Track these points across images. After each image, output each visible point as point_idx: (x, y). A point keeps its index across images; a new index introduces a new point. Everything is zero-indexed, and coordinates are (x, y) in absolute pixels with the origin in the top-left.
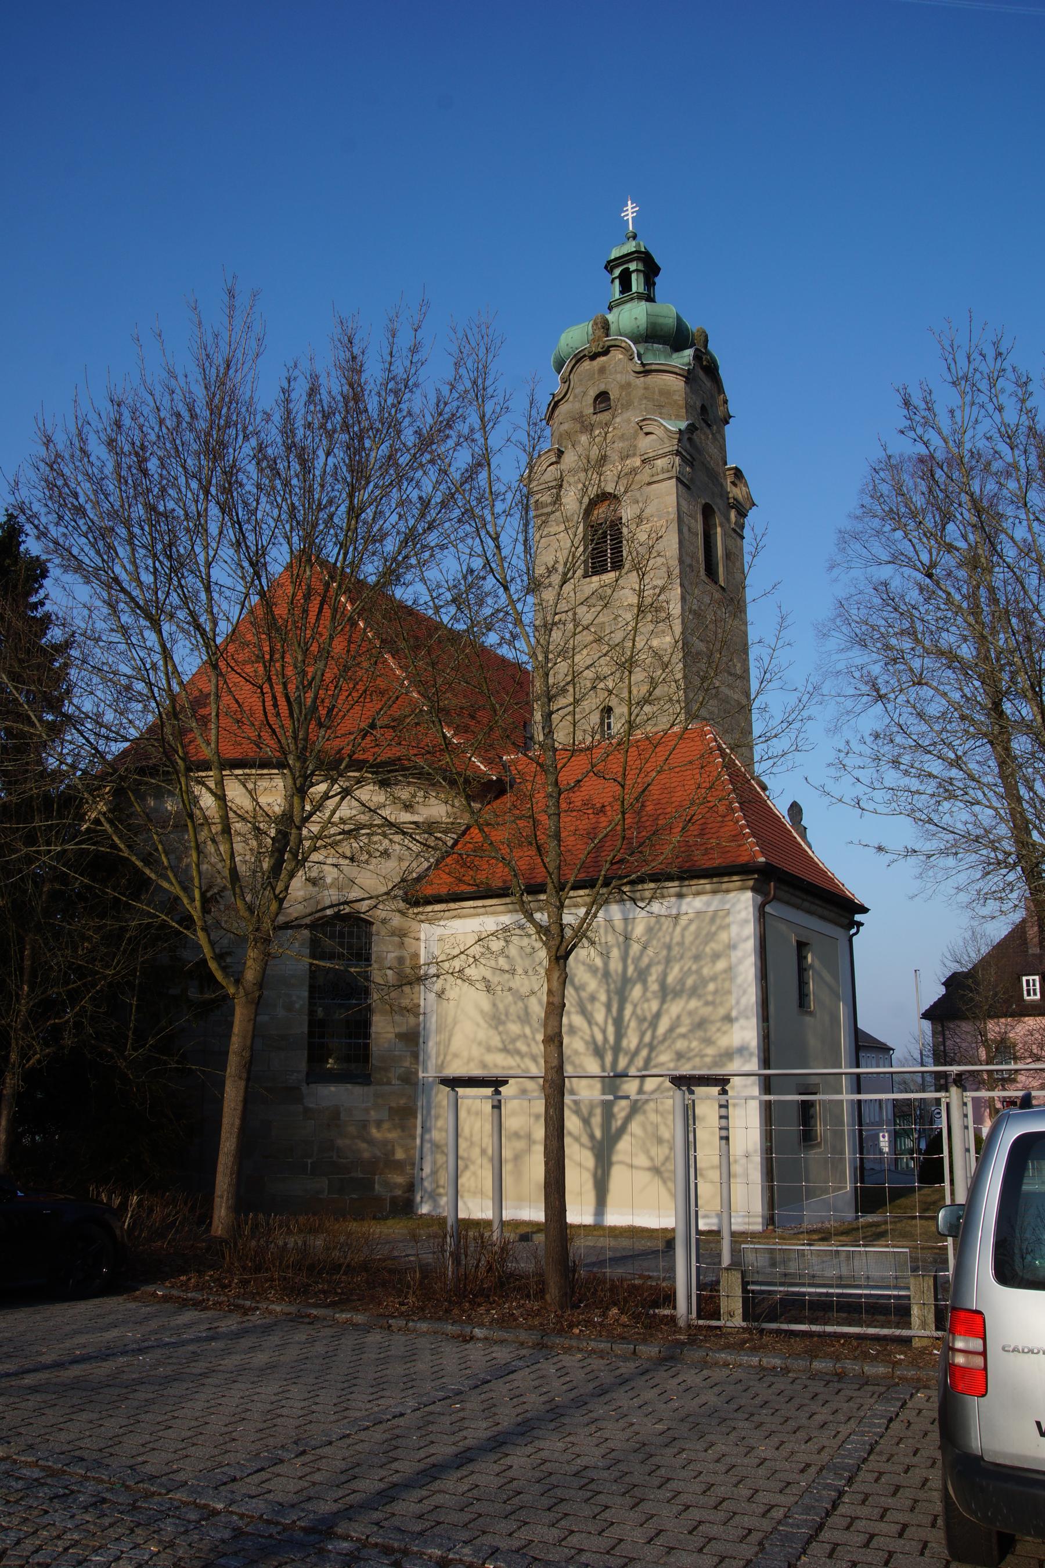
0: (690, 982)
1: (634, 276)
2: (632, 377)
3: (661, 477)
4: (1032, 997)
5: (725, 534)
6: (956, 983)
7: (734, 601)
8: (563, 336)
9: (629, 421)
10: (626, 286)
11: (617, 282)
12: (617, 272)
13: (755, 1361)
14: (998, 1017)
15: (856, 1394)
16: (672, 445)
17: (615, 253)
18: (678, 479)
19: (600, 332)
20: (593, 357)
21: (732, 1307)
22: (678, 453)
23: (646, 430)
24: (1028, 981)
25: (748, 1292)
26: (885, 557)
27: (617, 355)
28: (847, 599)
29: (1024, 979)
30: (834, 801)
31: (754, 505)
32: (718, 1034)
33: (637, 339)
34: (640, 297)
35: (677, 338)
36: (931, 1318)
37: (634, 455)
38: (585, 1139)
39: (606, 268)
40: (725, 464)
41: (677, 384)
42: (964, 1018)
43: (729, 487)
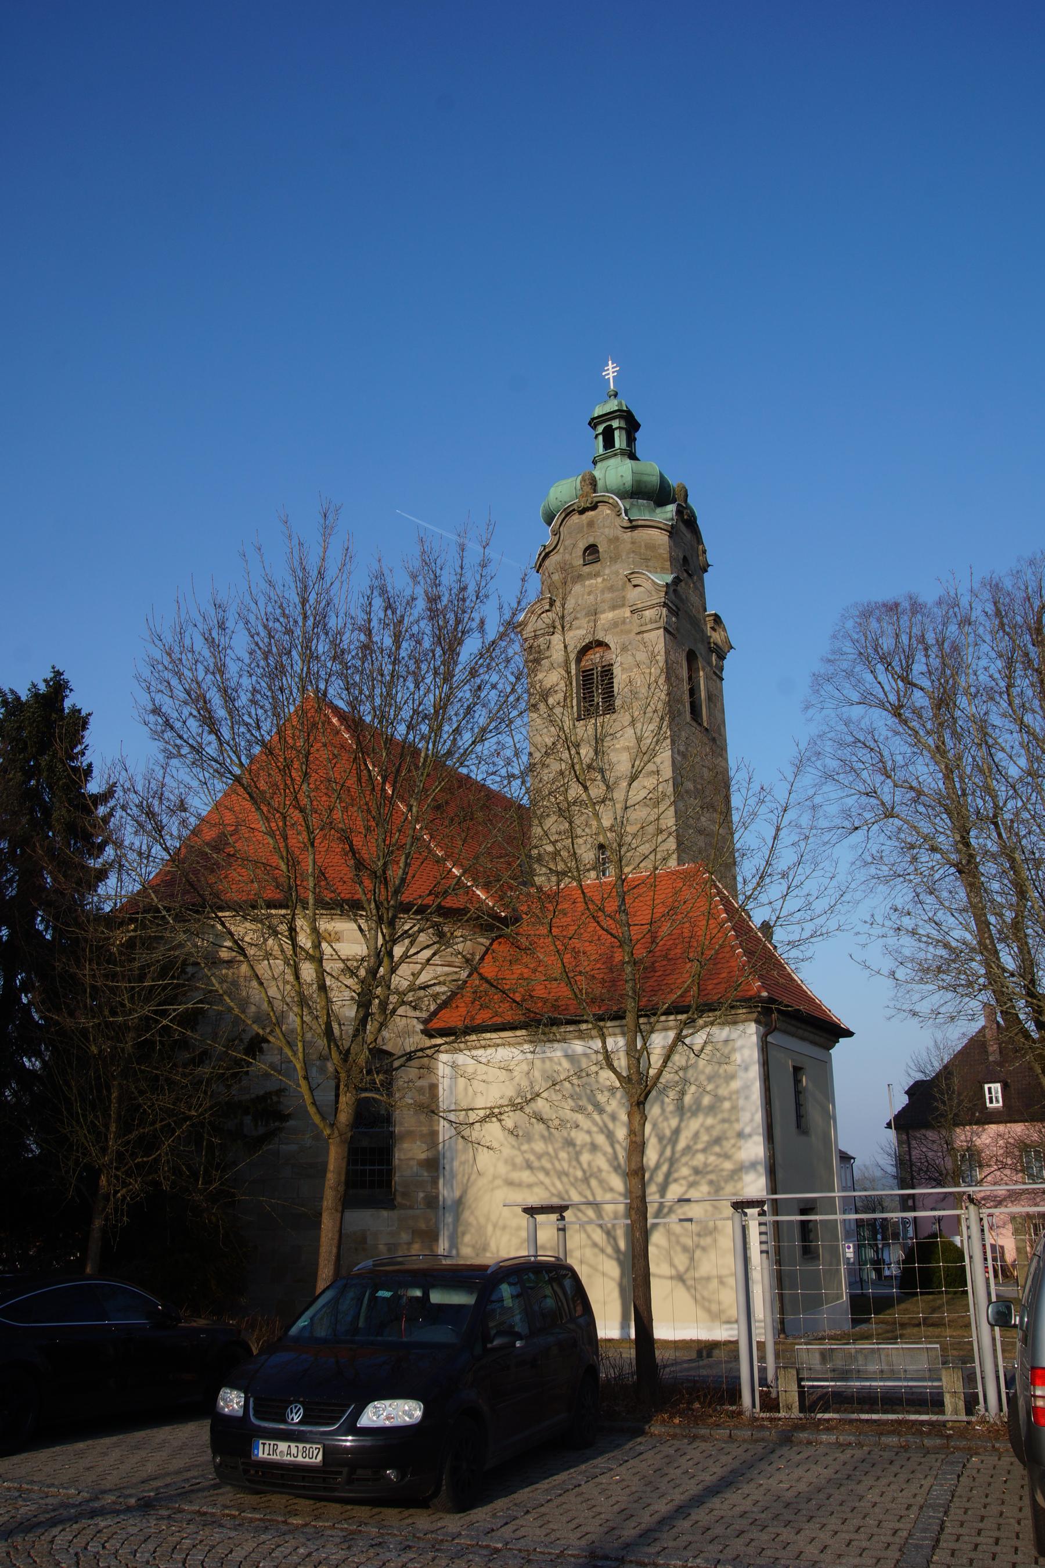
0: (706, 1100)
1: (617, 433)
2: (619, 532)
3: (649, 627)
4: (995, 1105)
5: (707, 677)
6: (918, 1092)
7: (715, 739)
8: (552, 490)
9: (617, 573)
10: (609, 442)
11: (601, 438)
12: (600, 429)
13: (833, 1438)
14: (964, 1125)
15: (923, 1460)
16: (660, 597)
17: (598, 411)
18: (665, 629)
19: (588, 489)
20: (582, 512)
21: (790, 1401)
22: (665, 605)
23: (634, 583)
24: (990, 1089)
25: (804, 1387)
26: (855, 697)
27: (604, 511)
28: (820, 736)
29: (986, 1086)
30: (873, 973)
31: (732, 648)
32: (733, 1150)
33: (623, 495)
34: (623, 453)
35: (660, 494)
36: (961, 1404)
37: (623, 605)
38: (609, 1250)
39: (590, 424)
40: (705, 610)
41: (661, 538)
42: (928, 1126)
43: (709, 632)
